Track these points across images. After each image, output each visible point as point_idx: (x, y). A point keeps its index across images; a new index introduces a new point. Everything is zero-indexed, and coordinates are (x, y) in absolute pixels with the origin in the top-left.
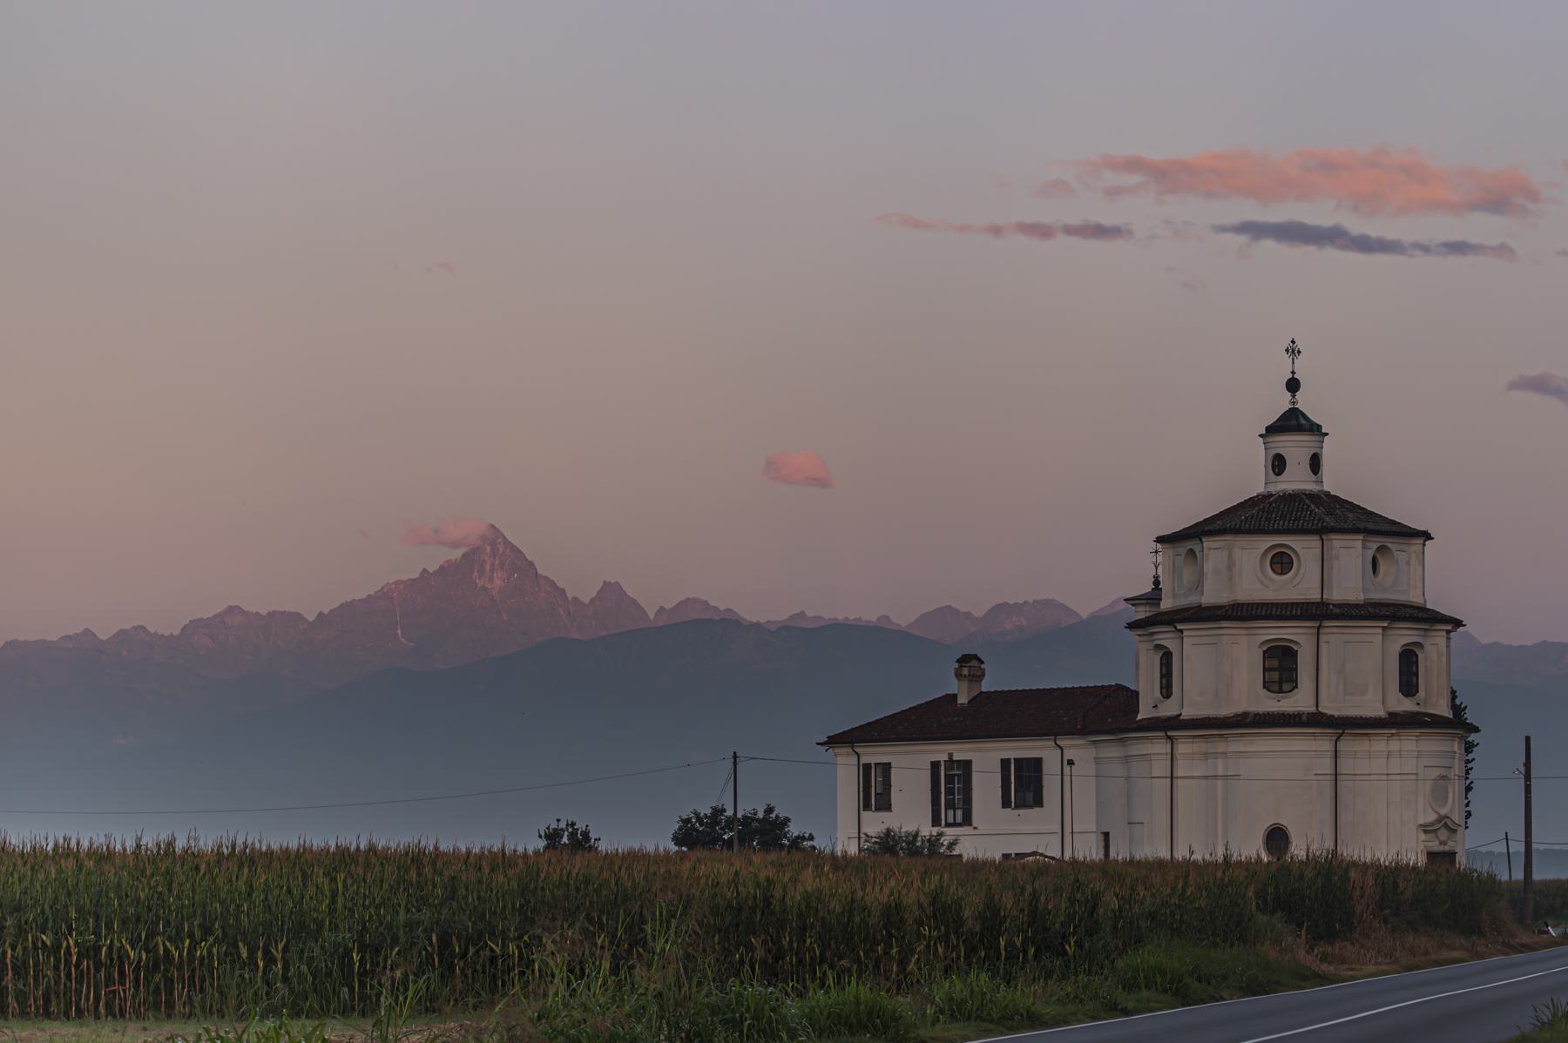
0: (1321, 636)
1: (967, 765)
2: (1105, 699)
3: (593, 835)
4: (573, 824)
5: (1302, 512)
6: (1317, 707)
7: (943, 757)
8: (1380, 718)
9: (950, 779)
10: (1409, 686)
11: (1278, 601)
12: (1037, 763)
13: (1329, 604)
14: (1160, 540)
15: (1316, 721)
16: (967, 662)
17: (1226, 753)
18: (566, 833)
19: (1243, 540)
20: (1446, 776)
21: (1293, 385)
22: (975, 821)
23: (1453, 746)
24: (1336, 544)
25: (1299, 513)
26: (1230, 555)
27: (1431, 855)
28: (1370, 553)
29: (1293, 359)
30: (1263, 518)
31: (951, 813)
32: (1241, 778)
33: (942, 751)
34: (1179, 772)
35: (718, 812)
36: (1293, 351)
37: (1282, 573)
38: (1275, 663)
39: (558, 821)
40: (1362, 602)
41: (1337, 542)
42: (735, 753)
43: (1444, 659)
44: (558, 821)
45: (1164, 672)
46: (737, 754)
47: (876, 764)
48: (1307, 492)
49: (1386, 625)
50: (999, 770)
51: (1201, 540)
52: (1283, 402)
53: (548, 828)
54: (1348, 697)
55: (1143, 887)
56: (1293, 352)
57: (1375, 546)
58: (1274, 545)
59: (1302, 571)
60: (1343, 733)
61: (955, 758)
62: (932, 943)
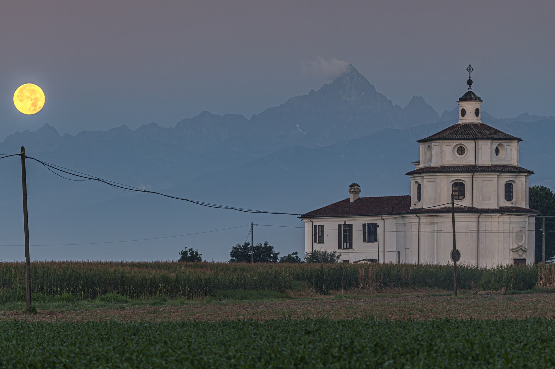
0: (474, 179)
1: (351, 226)
2: (402, 201)
3: (199, 253)
4: (191, 249)
5: (469, 131)
6: (472, 205)
7: (342, 223)
8: (496, 209)
9: (345, 231)
10: (509, 195)
11: (459, 165)
12: (376, 226)
13: (477, 166)
15: (471, 210)
16: (353, 187)
17: (437, 222)
18: (189, 253)
19: (446, 142)
20: (522, 231)
21: (470, 82)
22: (354, 247)
23: (526, 220)
24: (480, 144)
25: (468, 132)
26: (441, 148)
27: (515, 260)
28: (494, 147)
29: (470, 72)
30: (455, 134)
31: (345, 244)
32: (443, 232)
33: (341, 221)
34: (421, 229)
35: (247, 244)
36: (470, 69)
37: (461, 155)
38: (457, 188)
39: (186, 248)
40: (490, 166)
41: (481, 143)
42: (252, 223)
43: (524, 187)
44: (186, 248)
46: (253, 224)
47: (319, 225)
48: (473, 124)
49: (498, 174)
50: (362, 230)
51: (431, 142)
53: (182, 251)
54: (483, 201)
56: (470, 70)
57: (497, 144)
58: (457, 144)
59: (468, 153)
60: (480, 215)
61: (347, 223)
62: (162, 288)
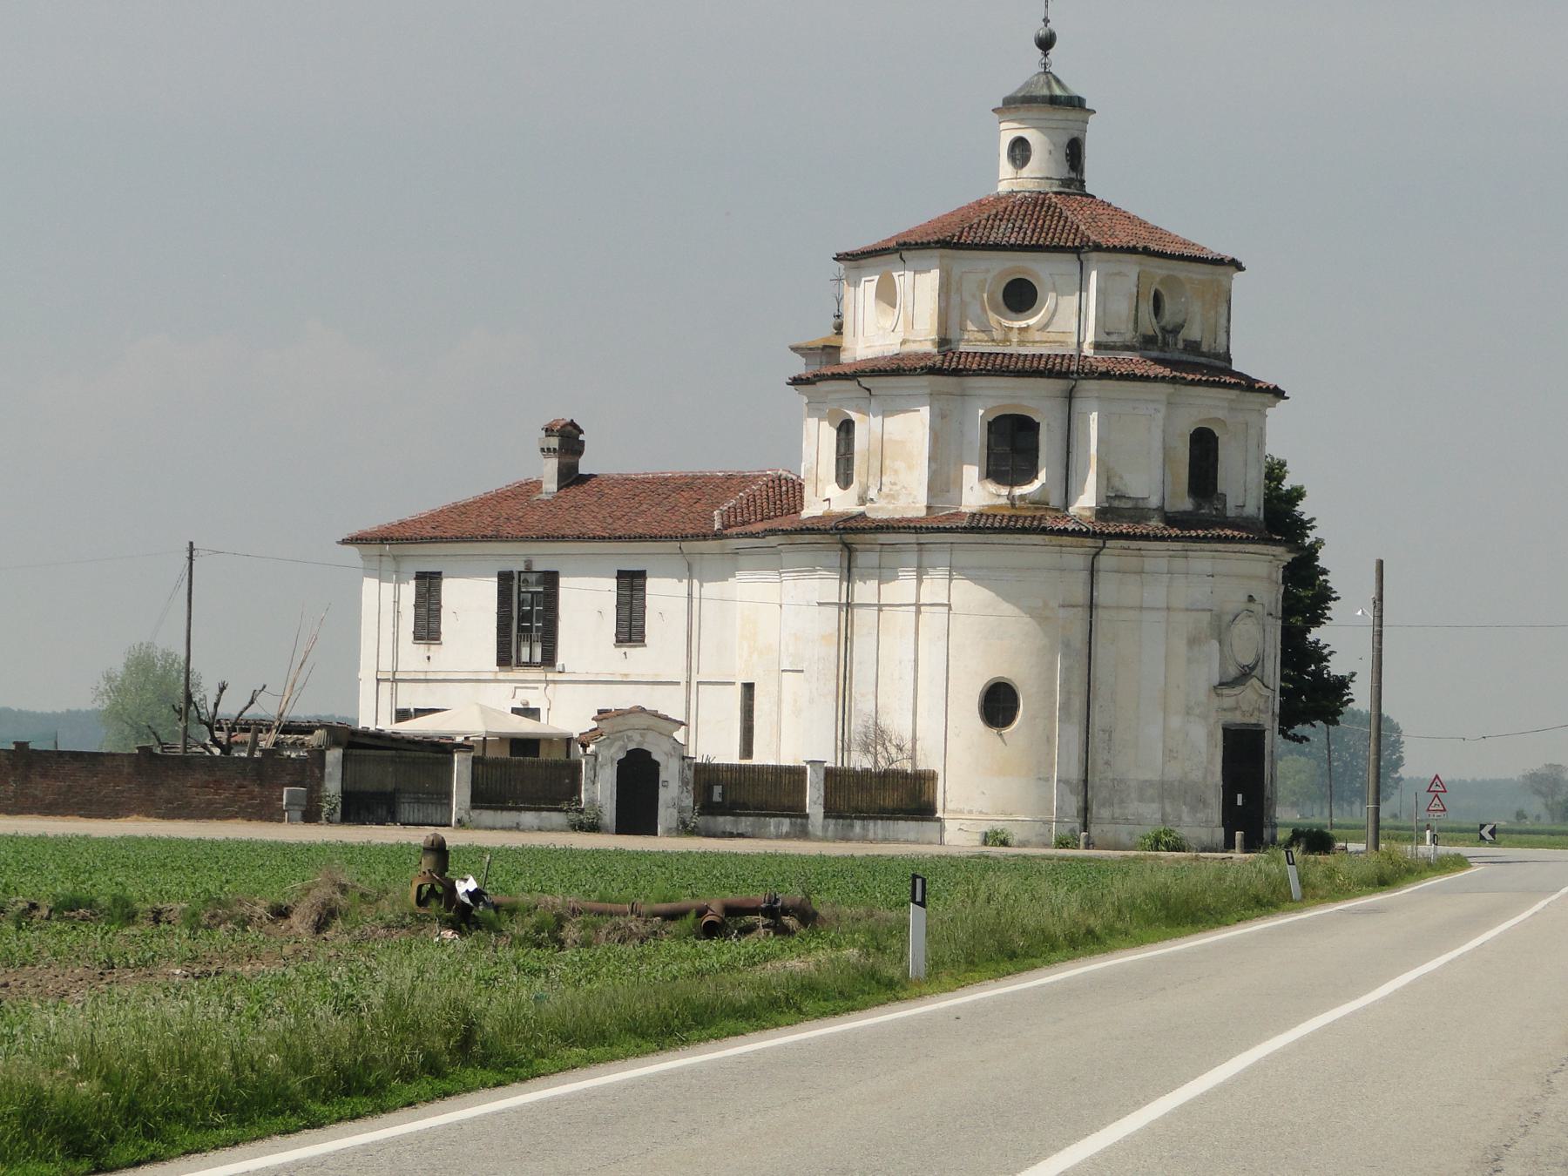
14: (839, 258)
21: (1046, 21)
42: (191, 544)
45: (842, 451)
52: (1023, 69)
55: (35, 912)
60: (1104, 547)
